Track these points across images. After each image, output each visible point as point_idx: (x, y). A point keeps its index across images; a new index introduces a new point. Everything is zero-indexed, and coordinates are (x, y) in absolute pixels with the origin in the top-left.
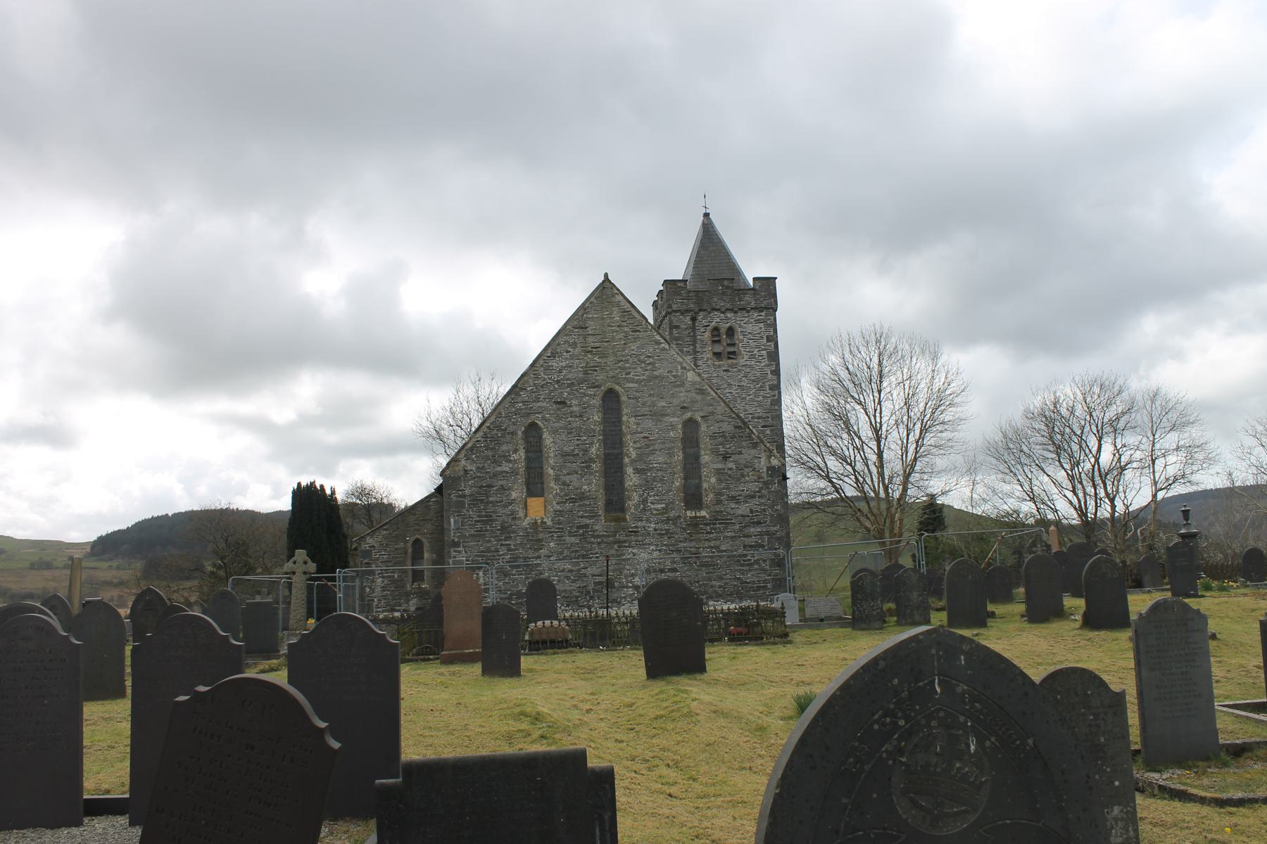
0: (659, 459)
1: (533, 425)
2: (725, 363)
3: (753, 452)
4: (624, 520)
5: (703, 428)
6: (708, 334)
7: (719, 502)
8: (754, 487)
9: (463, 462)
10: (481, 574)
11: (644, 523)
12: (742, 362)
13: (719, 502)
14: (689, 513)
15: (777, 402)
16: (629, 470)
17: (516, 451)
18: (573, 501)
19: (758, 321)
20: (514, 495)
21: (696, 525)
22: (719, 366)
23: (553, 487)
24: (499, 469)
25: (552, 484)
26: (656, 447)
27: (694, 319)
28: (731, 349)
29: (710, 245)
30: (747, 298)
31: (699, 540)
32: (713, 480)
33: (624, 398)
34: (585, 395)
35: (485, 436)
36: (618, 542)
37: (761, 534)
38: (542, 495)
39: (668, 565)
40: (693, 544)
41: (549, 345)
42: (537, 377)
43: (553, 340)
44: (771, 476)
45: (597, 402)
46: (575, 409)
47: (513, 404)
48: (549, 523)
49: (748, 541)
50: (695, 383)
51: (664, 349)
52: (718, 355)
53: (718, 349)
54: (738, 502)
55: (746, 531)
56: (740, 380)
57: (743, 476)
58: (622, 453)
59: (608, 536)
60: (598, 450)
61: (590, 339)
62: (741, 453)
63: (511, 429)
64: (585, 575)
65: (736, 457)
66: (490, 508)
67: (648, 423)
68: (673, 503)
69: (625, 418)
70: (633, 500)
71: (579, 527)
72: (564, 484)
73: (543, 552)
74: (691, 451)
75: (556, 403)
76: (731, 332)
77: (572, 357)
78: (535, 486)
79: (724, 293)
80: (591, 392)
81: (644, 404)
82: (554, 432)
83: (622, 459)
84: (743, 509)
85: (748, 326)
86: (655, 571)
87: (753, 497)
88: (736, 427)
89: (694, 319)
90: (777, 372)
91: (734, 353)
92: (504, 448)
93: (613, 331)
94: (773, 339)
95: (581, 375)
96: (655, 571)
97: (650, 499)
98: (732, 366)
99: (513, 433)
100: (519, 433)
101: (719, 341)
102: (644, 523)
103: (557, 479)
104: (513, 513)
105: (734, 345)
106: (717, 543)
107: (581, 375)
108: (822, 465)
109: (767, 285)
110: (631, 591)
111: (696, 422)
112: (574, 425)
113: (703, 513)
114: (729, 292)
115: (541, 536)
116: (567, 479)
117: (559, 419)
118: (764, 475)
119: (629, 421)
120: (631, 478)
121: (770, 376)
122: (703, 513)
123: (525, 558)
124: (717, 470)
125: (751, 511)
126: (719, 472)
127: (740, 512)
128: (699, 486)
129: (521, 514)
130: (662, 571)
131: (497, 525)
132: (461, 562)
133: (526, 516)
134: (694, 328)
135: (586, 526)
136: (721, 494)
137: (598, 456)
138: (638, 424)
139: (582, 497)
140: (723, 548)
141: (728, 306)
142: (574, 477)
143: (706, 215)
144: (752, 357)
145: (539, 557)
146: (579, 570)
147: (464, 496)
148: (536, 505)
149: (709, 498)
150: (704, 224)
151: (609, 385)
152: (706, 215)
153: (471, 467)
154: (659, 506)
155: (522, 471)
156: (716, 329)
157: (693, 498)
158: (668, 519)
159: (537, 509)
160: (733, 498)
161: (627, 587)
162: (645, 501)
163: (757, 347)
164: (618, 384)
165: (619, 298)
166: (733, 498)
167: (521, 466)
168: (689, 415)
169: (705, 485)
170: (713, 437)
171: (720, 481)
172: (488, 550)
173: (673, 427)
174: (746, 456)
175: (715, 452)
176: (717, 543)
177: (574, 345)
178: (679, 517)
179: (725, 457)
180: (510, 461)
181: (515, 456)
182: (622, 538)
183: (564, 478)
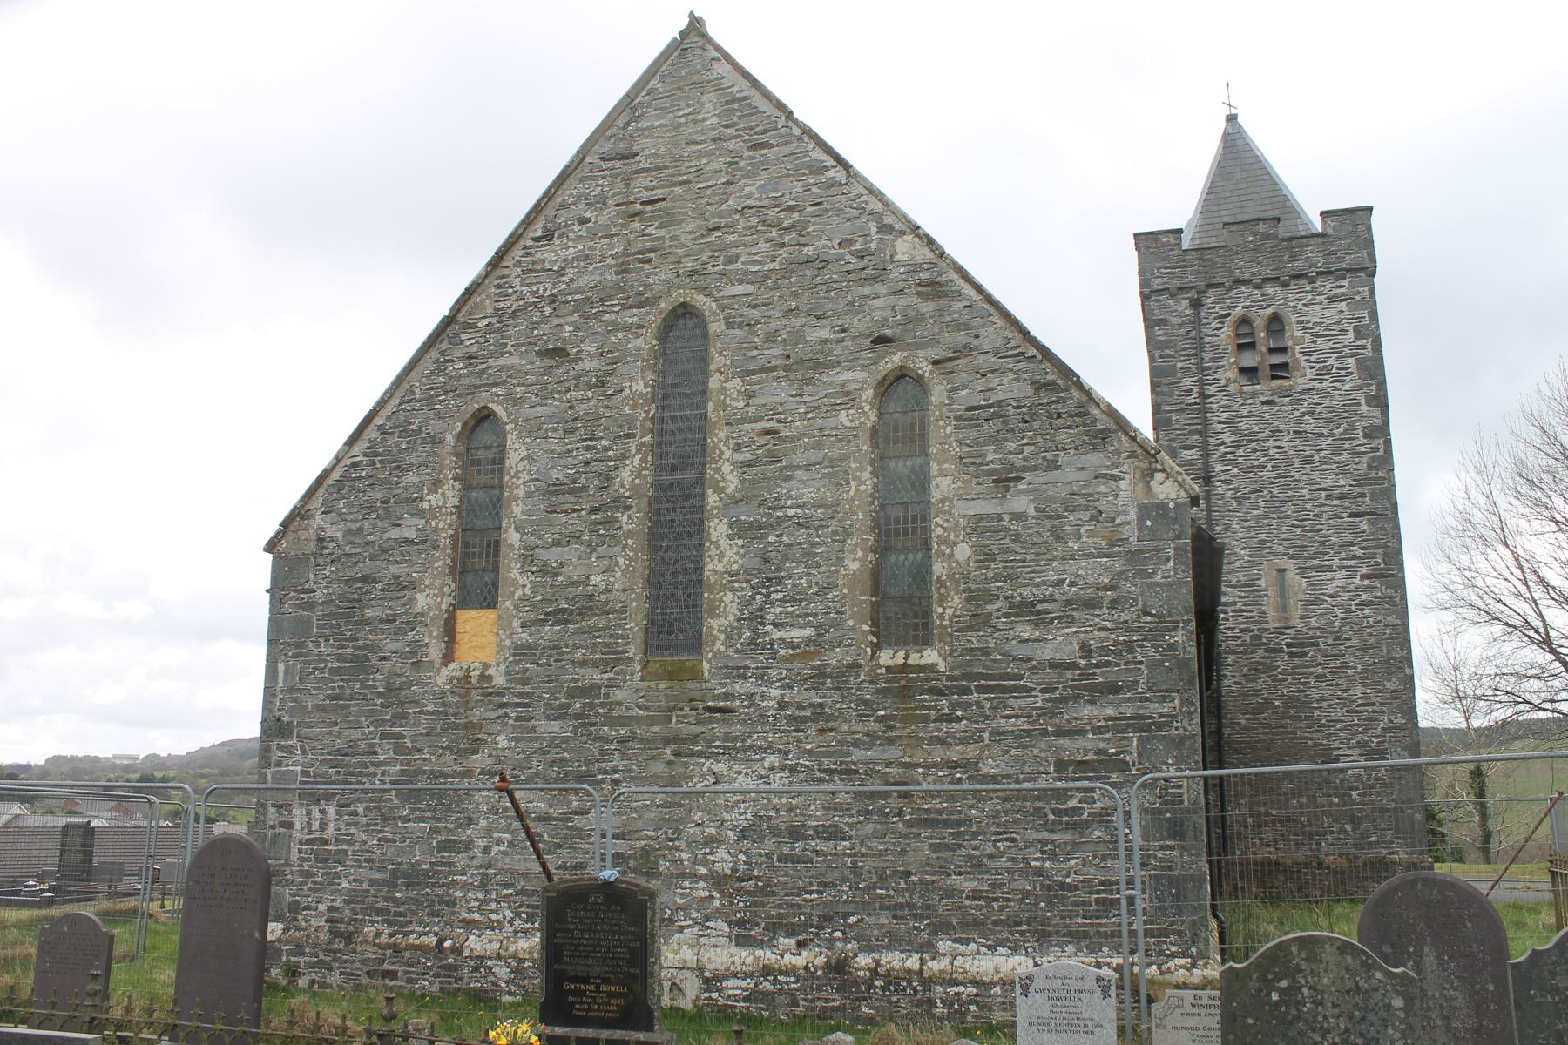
0: (806, 489)
1: (484, 417)
2: (1266, 387)
3: (1094, 460)
4: (696, 675)
5: (938, 393)
6: (1227, 332)
7: (979, 621)
8: (1094, 572)
9: (318, 519)
10: (331, 811)
11: (750, 686)
12: (1301, 383)
13: (979, 621)
14: (886, 657)
15: (1384, 462)
16: (718, 529)
17: (436, 485)
18: (561, 617)
19: (1333, 299)
20: (422, 601)
21: (905, 693)
22: (1253, 395)
23: (516, 578)
24: (394, 534)
25: (514, 574)
26: (799, 457)
27: (1196, 304)
28: (1278, 359)
29: (1237, 158)
30: (1308, 253)
31: (913, 741)
32: (963, 552)
33: (716, 327)
34: (616, 327)
35: (372, 452)
36: (677, 739)
37: (1116, 726)
38: (492, 605)
39: (816, 815)
40: (893, 753)
41: (537, 209)
42: (503, 292)
43: (549, 195)
44: (1153, 534)
45: (644, 343)
46: (587, 365)
47: (441, 366)
48: (500, 680)
49: (1071, 747)
50: (916, 267)
51: (832, 184)
52: (1249, 372)
53: (1249, 360)
54: (1041, 619)
55: (1068, 714)
56: (1299, 421)
57: (1059, 537)
58: (701, 482)
59: (651, 721)
60: (638, 474)
61: (642, 182)
62: (1053, 466)
63: (433, 427)
64: (580, 834)
65: (1040, 478)
66: (366, 636)
67: (778, 393)
68: (836, 625)
69: (714, 382)
70: (724, 614)
71: (573, 694)
72: (545, 571)
73: (480, 760)
74: (901, 467)
75: (544, 354)
76: (1276, 323)
77: (592, 235)
78: (476, 580)
79: (1257, 249)
80: (632, 317)
81: (770, 339)
82: (533, 430)
83: (703, 496)
84: (1059, 644)
85: (1312, 314)
86: (775, 832)
87: (1090, 604)
88: (1039, 387)
89: (1196, 304)
90: (1380, 401)
91: (1284, 366)
92: (411, 479)
93: (699, 154)
94: (1369, 332)
95: (610, 276)
96: (775, 832)
97: (772, 613)
98: (1280, 393)
99: (436, 441)
100: (449, 438)
101: (1252, 346)
102: (750, 686)
103: (527, 556)
104: (417, 649)
105: (1284, 350)
106: (972, 751)
107: (610, 276)
108: (1537, 623)
109: (1353, 224)
110: (702, 889)
111: (918, 380)
112: (581, 409)
113: (931, 656)
114: (1269, 244)
115: (477, 715)
116: (552, 556)
117: (544, 394)
118: (1131, 533)
119: (725, 388)
120: (723, 551)
121: (1364, 408)
122: (931, 656)
123: (437, 775)
124: (979, 519)
125: (1086, 650)
126: (981, 526)
127: (1046, 653)
128: (922, 575)
129: (435, 653)
130: (796, 833)
131: (378, 682)
132: (290, 776)
133: (448, 657)
134: (1197, 322)
135: (591, 690)
136: (985, 595)
137: (634, 489)
138: (750, 396)
139: (588, 606)
140: (988, 768)
141: (1269, 273)
142: (571, 553)
143: (1231, 119)
144: (1323, 373)
145: (467, 774)
146: (566, 817)
147: (311, 606)
148: (476, 625)
149: (949, 608)
150: (1225, 135)
151: (678, 296)
152: (1231, 119)
153: (334, 531)
154: (796, 634)
155: (445, 537)
156: (1244, 321)
157: (900, 607)
158: (821, 674)
159: (483, 639)
160: (1025, 609)
161: (694, 876)
162: (758, 617)
163: (1333, 351)
164: (704, 290)
165: (722, 68)
166: (1025, 609)
167: (445, 526)
168: (896, 359)
169: (939, 568)
170: (969, 418)
171: (985, 555)
172: (351, 748)
173: (849, 398)
174: (1070, 474)
175: (970, 464)
176: (972, 751)
177: (601, 202)
178: (855, 666)
179: (1004, 481)
180: (420, 513)
181: (432, 500)
182: (686, 730)
183: (543, 554)
